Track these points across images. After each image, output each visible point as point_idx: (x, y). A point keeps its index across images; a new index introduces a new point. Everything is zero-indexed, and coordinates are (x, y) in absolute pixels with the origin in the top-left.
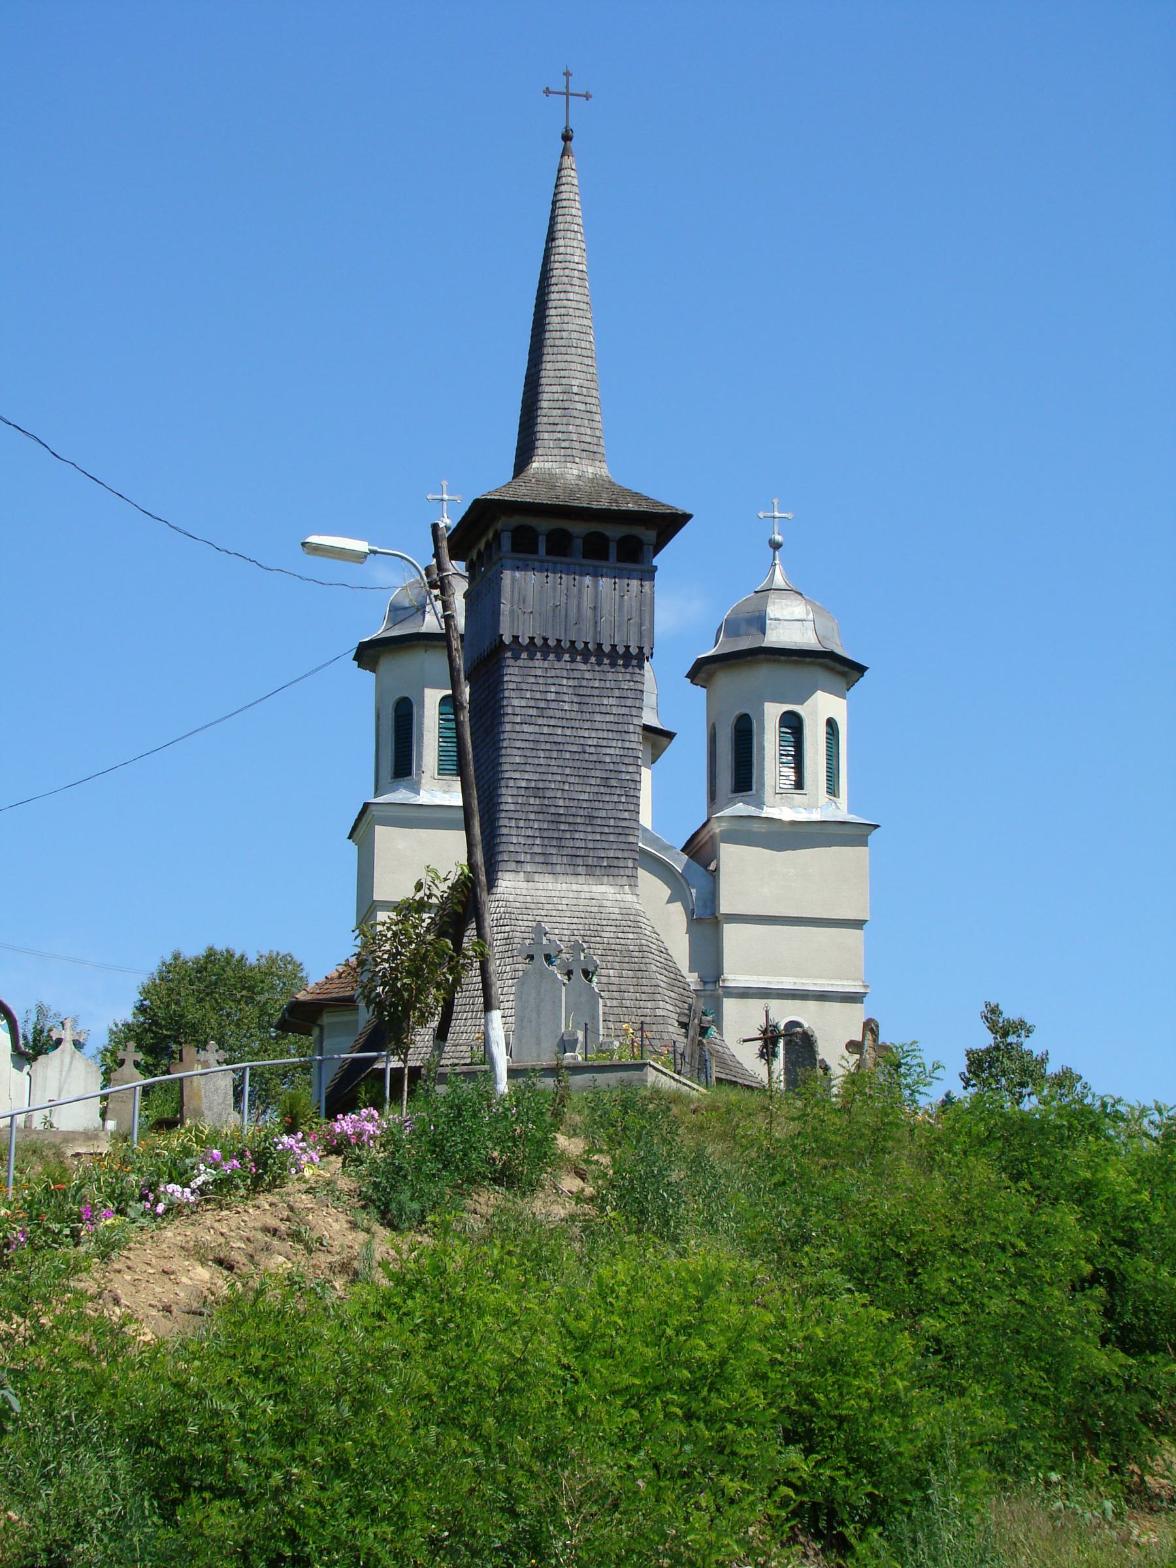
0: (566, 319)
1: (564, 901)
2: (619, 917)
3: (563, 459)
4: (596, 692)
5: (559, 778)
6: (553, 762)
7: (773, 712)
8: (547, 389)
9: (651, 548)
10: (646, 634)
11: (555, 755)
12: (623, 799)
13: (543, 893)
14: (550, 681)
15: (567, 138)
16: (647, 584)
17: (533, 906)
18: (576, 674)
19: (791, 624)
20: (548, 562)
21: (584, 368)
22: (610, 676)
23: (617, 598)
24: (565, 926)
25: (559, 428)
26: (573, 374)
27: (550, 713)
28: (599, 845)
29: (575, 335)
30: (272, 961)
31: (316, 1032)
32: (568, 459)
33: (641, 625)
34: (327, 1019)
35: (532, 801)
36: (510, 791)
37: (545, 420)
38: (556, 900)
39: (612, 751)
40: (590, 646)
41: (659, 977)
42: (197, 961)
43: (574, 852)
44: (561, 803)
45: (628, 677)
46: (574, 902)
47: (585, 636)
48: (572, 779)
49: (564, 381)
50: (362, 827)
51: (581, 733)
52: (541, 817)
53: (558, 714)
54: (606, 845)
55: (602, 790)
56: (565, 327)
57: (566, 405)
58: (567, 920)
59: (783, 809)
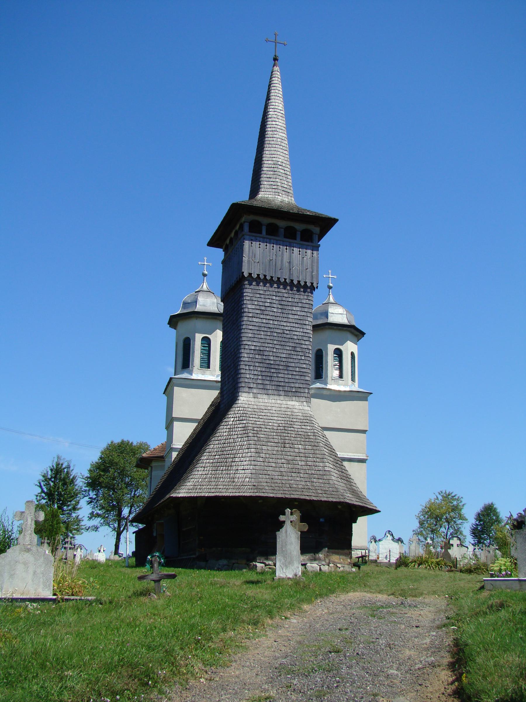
0: (275, 133)
1: (274, 409)
2: (302, 418)
3: (274, 194)
4: (290, 304)
5: (271, 345)
6: (268, 337)
7: (331, 348)
8: (266, 162)
9: (317, 236)
10: (315, 276)
11: (269, 334)
12: (303, 358)
13: (263, 404)
14: (267, 297)
15: (275, 59)
16: (315, 252)
17: (257, 410)
18: (280, 294)
19: (338, 315)
20: (267, 238)
21: (284, 155)
22: (297, 296)
23: (301, 258)
24: (275, 421)
25: (271, 180)
26: (278, 156)
27: (267, 313)
28: (291, 381)
29: (279, 140)
30: (141, 444)
31: (150, 468)
32: (276, 194)
33: (312, 272)
34: (154, 464)
35: (257, 356)
36: (246, 351)
37: (265, 176)
38: (269, 408)
39: (297, 333)
40: (287, 281)
41: (325, 450)
42: (118, 444)
43: (278, 384)
44: (272, 358)
45: (306, 297)
46: (279, 409)
47: (285, 276)
48: (277, 347)
49: (274, 159)
50: (168, 390)
51: (282, 323)
52: (261, 365)
53: (271, 313)
54: (294, 381)
55: (293, 353)
56: (275, 136)
57: (275, 169)
58: (276, 418)
59: (333, 386)
